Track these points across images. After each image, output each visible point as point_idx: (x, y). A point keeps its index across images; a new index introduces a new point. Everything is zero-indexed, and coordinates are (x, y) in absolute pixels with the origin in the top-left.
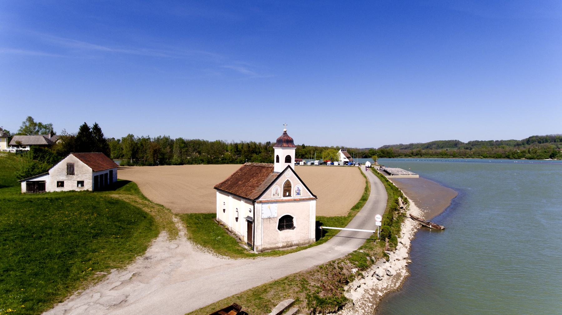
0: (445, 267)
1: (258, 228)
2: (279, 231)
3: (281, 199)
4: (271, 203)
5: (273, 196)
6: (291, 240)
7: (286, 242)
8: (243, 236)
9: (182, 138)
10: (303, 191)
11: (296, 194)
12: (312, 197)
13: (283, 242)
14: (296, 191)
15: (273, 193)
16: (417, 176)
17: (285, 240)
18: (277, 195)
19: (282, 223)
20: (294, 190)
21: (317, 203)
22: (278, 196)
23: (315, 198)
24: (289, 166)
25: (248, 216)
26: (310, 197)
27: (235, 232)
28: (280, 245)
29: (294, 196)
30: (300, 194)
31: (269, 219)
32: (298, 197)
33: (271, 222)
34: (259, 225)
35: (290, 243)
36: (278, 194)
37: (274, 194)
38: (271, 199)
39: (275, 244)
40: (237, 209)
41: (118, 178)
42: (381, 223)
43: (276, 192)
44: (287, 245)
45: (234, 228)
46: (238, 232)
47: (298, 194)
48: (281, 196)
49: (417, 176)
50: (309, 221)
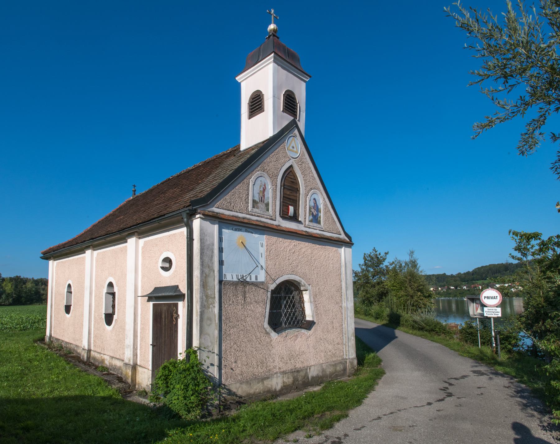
1: (206, 316)
2: (273, 335)
3: (275, 223)
4: (246, 231)
5: (253, 207)
6: (305, 364)
7: (292, 372)
8: (134, 367)
9: (20, 276)
10: (325, 213)
11: (311, 217)
12: (343, 236)
13: (284, 373)
14: (310, 211)
17: (289, 367)
21: (353, 252)
22: (268, 210)
23: (348, 240)
24: (293, 125)
25: (264, 111)
27: (103, 361)
28: (276, 383)
29: (307, 223)
31: (240, 288)
32: (315, 231)
33: (248, 300)
34: (209, 308)
35: (302, 374)
36: (267, 205)
37: (254, 201)
38: (248, 216)
39: (263, 379)
40: (134, 186)
42: (499, 310)
43: (261, 195)
44: (294, 382)
45: (99, 351)
46: (112, 357)
47: (316, 219)
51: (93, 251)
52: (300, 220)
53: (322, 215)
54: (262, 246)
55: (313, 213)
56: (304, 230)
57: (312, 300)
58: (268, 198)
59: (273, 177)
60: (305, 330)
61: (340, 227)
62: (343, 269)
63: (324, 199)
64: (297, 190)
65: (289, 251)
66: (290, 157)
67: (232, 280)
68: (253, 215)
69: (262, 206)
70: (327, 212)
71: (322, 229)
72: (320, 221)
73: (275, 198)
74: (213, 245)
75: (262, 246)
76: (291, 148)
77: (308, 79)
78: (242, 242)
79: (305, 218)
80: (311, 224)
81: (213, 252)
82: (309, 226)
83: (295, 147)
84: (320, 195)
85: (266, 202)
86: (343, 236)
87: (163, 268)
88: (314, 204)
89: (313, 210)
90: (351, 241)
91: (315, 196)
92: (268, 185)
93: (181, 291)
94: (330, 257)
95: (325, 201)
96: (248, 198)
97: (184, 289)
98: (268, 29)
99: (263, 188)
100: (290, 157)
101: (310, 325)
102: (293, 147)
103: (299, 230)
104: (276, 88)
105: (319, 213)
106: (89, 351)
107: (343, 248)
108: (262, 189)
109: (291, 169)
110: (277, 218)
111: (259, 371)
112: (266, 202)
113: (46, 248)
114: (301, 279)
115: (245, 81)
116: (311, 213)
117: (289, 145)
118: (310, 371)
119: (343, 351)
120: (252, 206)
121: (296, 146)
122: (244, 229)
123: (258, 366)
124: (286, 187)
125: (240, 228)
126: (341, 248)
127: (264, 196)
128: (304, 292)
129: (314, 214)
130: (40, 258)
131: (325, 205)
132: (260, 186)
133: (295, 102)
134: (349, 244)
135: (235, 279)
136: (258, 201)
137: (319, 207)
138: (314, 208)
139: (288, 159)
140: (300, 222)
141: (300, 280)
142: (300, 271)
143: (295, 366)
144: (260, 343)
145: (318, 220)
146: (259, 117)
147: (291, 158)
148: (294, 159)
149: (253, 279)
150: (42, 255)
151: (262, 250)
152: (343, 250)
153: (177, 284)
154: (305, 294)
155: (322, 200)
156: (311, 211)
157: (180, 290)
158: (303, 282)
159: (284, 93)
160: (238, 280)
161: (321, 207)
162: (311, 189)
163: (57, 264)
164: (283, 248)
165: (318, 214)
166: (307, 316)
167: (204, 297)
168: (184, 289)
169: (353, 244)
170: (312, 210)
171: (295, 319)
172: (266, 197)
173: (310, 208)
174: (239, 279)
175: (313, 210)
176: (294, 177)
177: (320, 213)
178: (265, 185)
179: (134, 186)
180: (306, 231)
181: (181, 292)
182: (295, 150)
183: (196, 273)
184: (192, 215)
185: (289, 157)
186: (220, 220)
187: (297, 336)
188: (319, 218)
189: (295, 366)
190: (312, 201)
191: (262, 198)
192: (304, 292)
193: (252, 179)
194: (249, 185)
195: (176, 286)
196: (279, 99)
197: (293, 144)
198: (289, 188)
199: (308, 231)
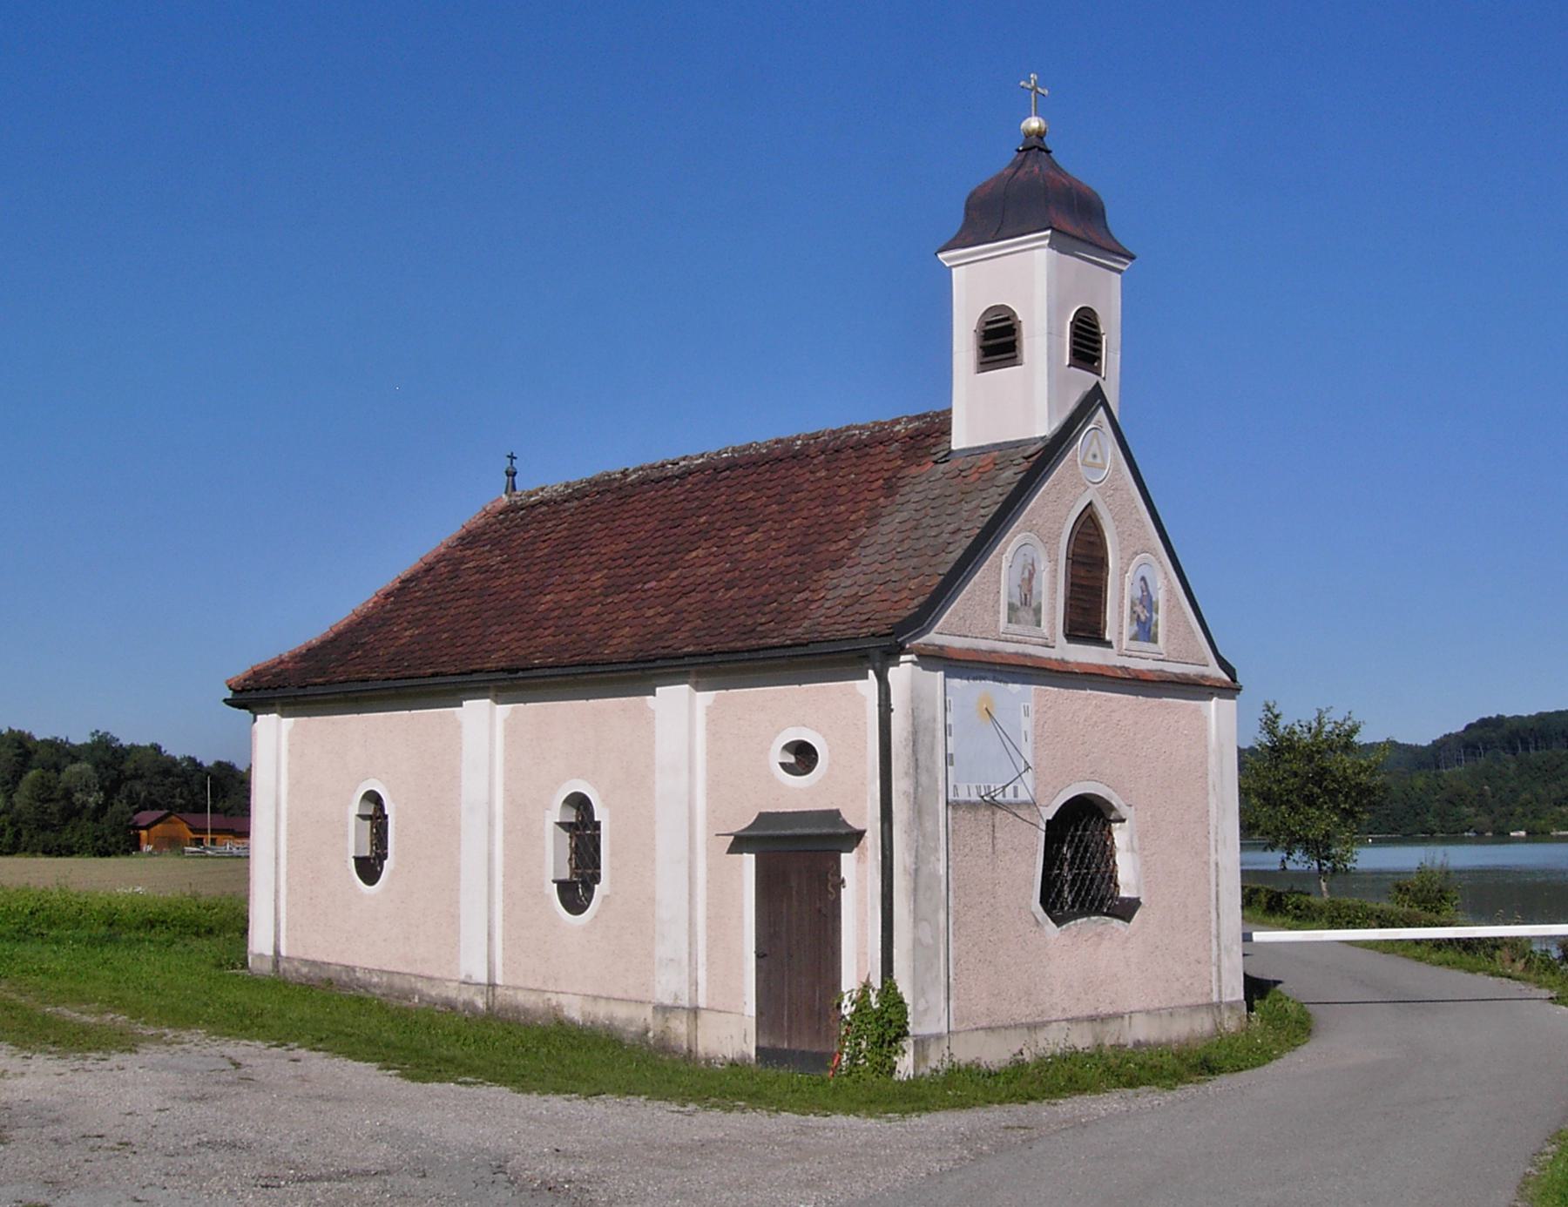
0: (815, 993)
3: (1054, 654)
4: (995, 679)
5: (1010, 621)
10: (1169, 612)
11: (1135, 628)
12: (1215, 672)
15: (1010, 596)
16: (1512, 834)
18: (1030, 616)
19: (1050, 897)
20: (1121, 606)
21: (1238, 706)
22: (1039, 624)
23: (1228, 679)
24: (1095, 398)
26: (1207, 671)
29: (1126, 643)
30: (1155, 641)
32: (1144, 661)
33: (1000, 845)
37: (1011, 607)
40: (512, 457)
41: (843, 855)
47: (1146, 631)
48: (1053, 634)
49: (1512, 834)
50: (1207, 863)
51: (493, 704)
52: (1108, 637)
53: (1161, 617)
54: (1027, 714)
55: (1139, 616)
56: (1118, 664)
57: (1136, 844)
58: (1040, 593)
59: (1049, 541)
60: (1121, 922)
61: (1207, 645)
62: (1212, 760)
63: (1166, 573)
64: (1102, 563)
65: (1085, 720)
66: (1087, 483)
67: (968, 799)
68: (1007, 641)
69: (1026, 616)
70: (1173, 606)
71: (1161, 657)
72: (1156, 635)
73: (1053, 599)
74: (935, 720)
75: (1027, 714)
76: (1090, 459)
77: (1126, 264)
78: (987, 709)
79: (1121, 633)
80: (1136, 645)
81: (934, 737)
82: (1129, 653)
83: (1099, 455)
84: (1156, 565)
85: (1034, 604)
86: (1215, 672)
87: (785, 767)
88: (1143, 591)
89: (1139, 609)
90: (1234, 680)
91: (1144, 571)
92: (1039, 562)
93: (849, 822)
94: (1181, 730)
95: (1169, 581)
96: (998, 601)
97: (865, 816)
98: (1023, 125)
99: (1030, 571)
100: (1087, 483)
101: (1126, 910)
102: (1095, 456)
103: (1107, 667)
104: (1055, 310)
105: (1154, 614)
106: (492, 985)
107: (1215, 699)
108: (1026, 575)
109: (1089, 509)
110: (1057, 640)
111: (1024, 1013)
112: (1034, 604)
113: (241, 666)
114: (1110, 791)
115: (964, 267)
116: (1135, 616)
117: (1086, 454)
118: (1130, 1023)
119: (1211, 981)
120: (1006, 620)
121: (1101, 452)
122: (989, 675)
123: (1020, 999)
124: (1079, 559)
125: (982, 674)
126: (1211, 700)
127: (1030, 590)
128: (1115, 826)
129: (1143, 618)
130: (224, 704)
131: (1170, 591)
132: (1024, 568)
133: (1098, 334)
134: (1230, 690)
135: (975, 798)
136: (1019, 604)
137: (1154, 599)
138: (1141, 603)
139: (1083, 488)
140: (1109, 644)
141: (1108, 795)
142: (1108, 771)
143: (1096, 1008)
144: (1023, 948)
145: (1152, 633)
146: (1002, 376)
147: (1090, 485)
148: (1097, 486)
149: (1010, 796)
150: (229, 695)
151: (1027, 724)
152: (1213, 706)
153: (834, 808)
154: (1120, 828)
155: (1164, 583)
156: (1135, 612)
157: (844, 821)
158: (1115, 801)
159: (1071, 319)
160: (979, 799)
161: (1160, 596)
162: (1136, 554)
163: (295, 723)
164: (1070, 715)
165: (1151, 616)
166: (1122, 887)
167: (920, 838)
168: (865, 816)
169: (1239, 690)
170: (1136, 608)
171: (1086, 893)
172: (1034, 592)
173: (1133, 604)
174: (982, 797)
175: (1139, 609)
176: (1097, 529)
177: (1157, 613)
178: (1033, 565)
179: (512, 457)
180: (1124, 667)
181: (850, 826)
182: (1099, 460)
183: (899, 785)
184: (891, 655)
185: (1084, 484)
186: (946, 663)
187: (1100, 935)
188: (1153, 628)
189: (1096, 1008)
190: (1138, 584)
191: (1026, 595)
192: (1115, 826)
193: (1006, 554)
194: (1000, 569)
195: (831, 811)
196: (1061, 335)
197: (1094, 449)
198: (1085, 560)
199: (1127, 665)
